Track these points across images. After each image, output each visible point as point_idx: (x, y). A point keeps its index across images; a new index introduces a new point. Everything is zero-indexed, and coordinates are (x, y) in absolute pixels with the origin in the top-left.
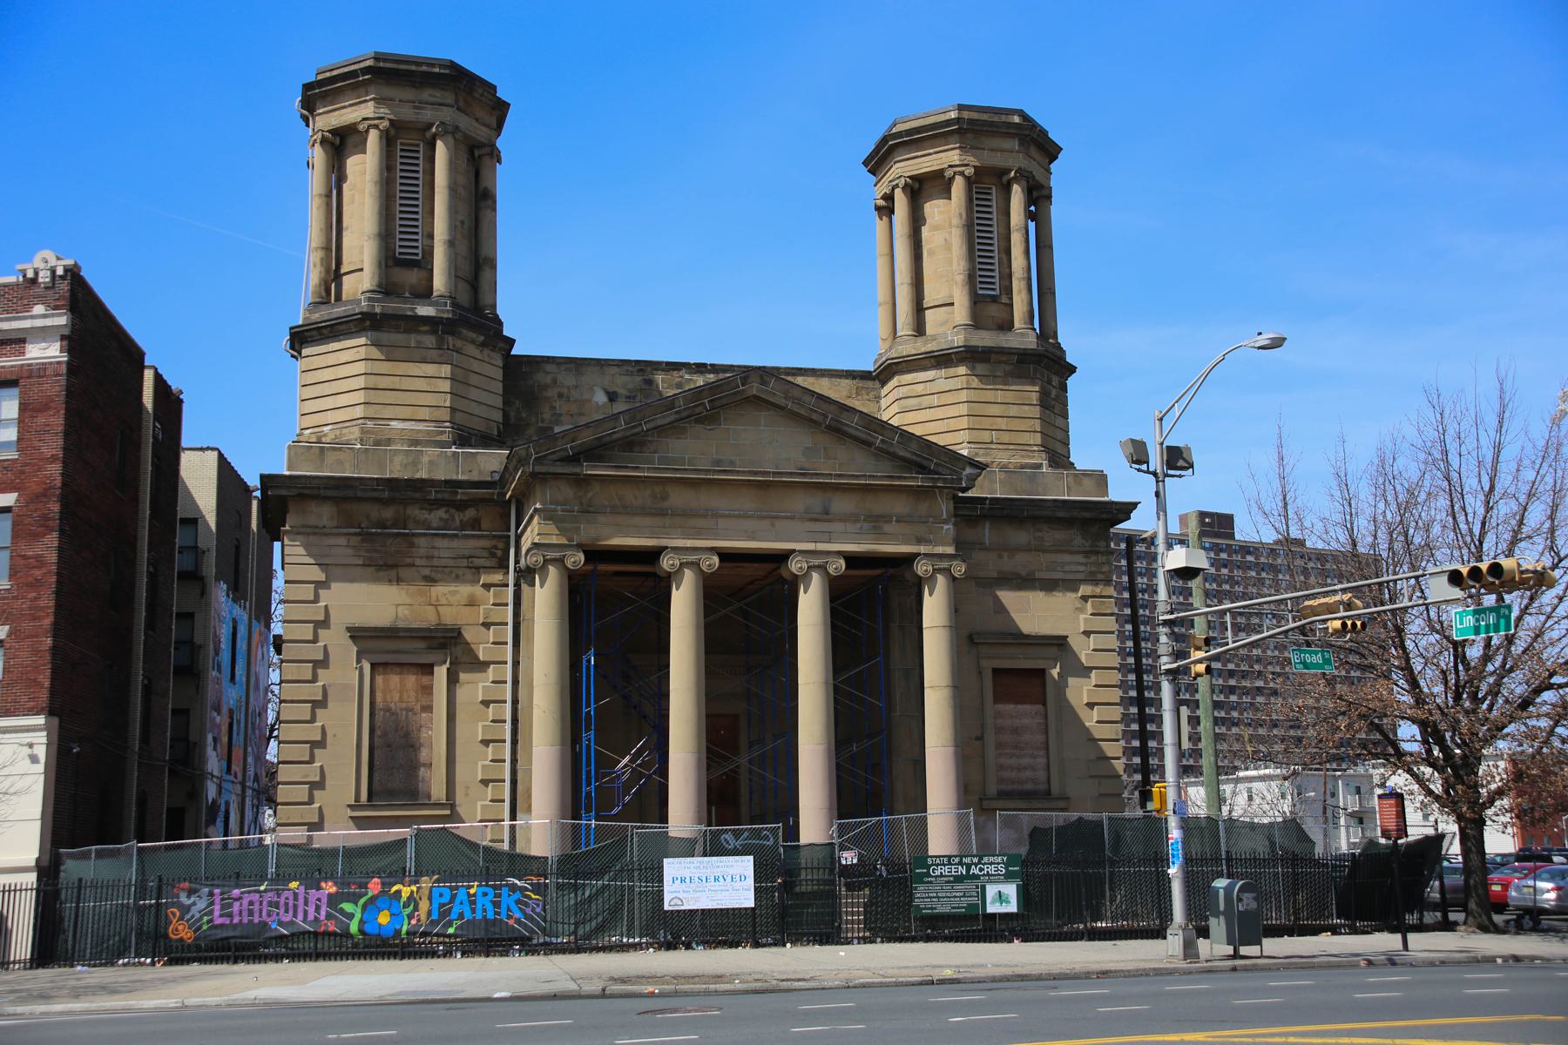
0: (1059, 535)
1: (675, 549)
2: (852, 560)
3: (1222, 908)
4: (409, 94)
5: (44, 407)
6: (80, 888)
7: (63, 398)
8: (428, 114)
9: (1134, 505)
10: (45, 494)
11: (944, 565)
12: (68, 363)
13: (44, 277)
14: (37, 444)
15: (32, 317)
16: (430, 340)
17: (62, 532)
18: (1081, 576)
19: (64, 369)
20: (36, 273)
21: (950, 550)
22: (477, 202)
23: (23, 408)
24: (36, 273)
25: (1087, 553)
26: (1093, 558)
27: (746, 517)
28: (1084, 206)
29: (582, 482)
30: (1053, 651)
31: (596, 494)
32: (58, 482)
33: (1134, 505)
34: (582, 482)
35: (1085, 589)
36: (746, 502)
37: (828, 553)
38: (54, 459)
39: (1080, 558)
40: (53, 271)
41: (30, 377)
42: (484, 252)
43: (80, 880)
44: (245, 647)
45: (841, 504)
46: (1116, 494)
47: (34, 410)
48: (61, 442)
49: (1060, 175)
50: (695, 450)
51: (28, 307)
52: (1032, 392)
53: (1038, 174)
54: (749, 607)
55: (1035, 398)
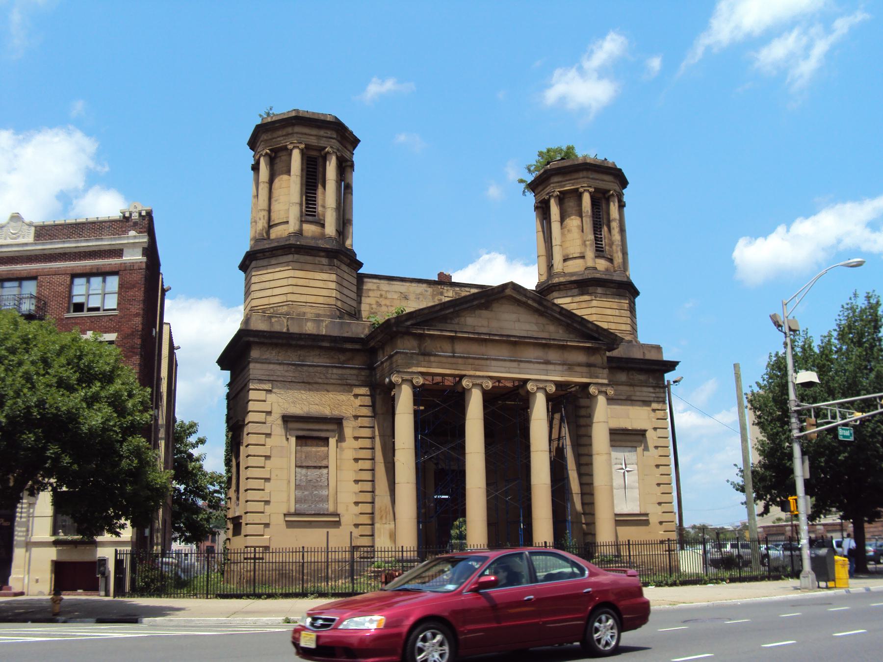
0: (642, 377)
1: (470, 376)
2: (558, 384)
3: (67, 597)
4: (314, 132)
5: (133, 286)
6: (629, 544)
7: (143, 282)
8: (322, 143)
9: (676, 363)
10: (132, 334)
11: (604, 389)
12: (146, 263)
13: (135, 216)
14: (129, 306)
15: (128, 238)
16: (324, 261)
17: (141, 356)
18: (652, 399)
19: (144, 266)
20: (131, 214)
21: (606, 381)
22: (345, 189)
23: (121, 286)
24: (131, 214)
25: (654, 387)
26: (657, 390)
27: (505, 360)
28: (638, 206)
29: (421, 337)
30: (640, 437)
31: (428, 345)
32: (140, 327)
33: (676, 363)
34: (421, 337)
35: (655, 406)
36: (503, 352)
37: (483, 377)
38: (137, 315)
39: (651, 390)
40: (140, 214)
41: (125, 270)
42: (347, 217)
43: (545, 543)
44: (553, 430)
45: (553, 355)
46: (667, 356)
47: (127, 288)
48: (141, 306)
49: (359, 156)
50: (476, 322)
51: (126, 232)
52: (366, 280)
53: (347, 155)
54: (507, 411)
55: (626, 306)
